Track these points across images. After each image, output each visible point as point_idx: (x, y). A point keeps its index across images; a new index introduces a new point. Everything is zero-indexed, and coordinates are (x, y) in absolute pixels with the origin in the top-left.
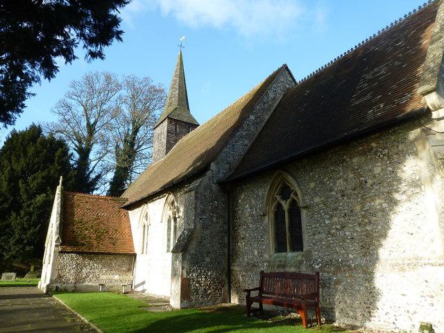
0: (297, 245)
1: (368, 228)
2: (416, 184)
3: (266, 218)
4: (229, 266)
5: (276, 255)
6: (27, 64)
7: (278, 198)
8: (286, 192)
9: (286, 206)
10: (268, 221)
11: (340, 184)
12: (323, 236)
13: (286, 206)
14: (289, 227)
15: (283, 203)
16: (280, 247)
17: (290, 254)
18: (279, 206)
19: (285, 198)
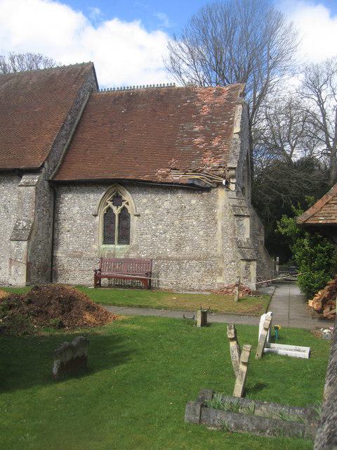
0: (125, 238)
1: (182, 234)
2: (46, 62)
3: (98, 218)
4: (52, 253)
5: (104, 246)
6: (322, 161)
7: (110, 204)
8: (117, 200)
9: (116, 211)
10: (99, 220)
11: (167, 205)
12: (149, 236)
13: (116, 211)
14: (119, 227)
15: (114, 208)
16: (108, 239)
17: (118, 247)
18: (109, 209)
19: (117, 205)
